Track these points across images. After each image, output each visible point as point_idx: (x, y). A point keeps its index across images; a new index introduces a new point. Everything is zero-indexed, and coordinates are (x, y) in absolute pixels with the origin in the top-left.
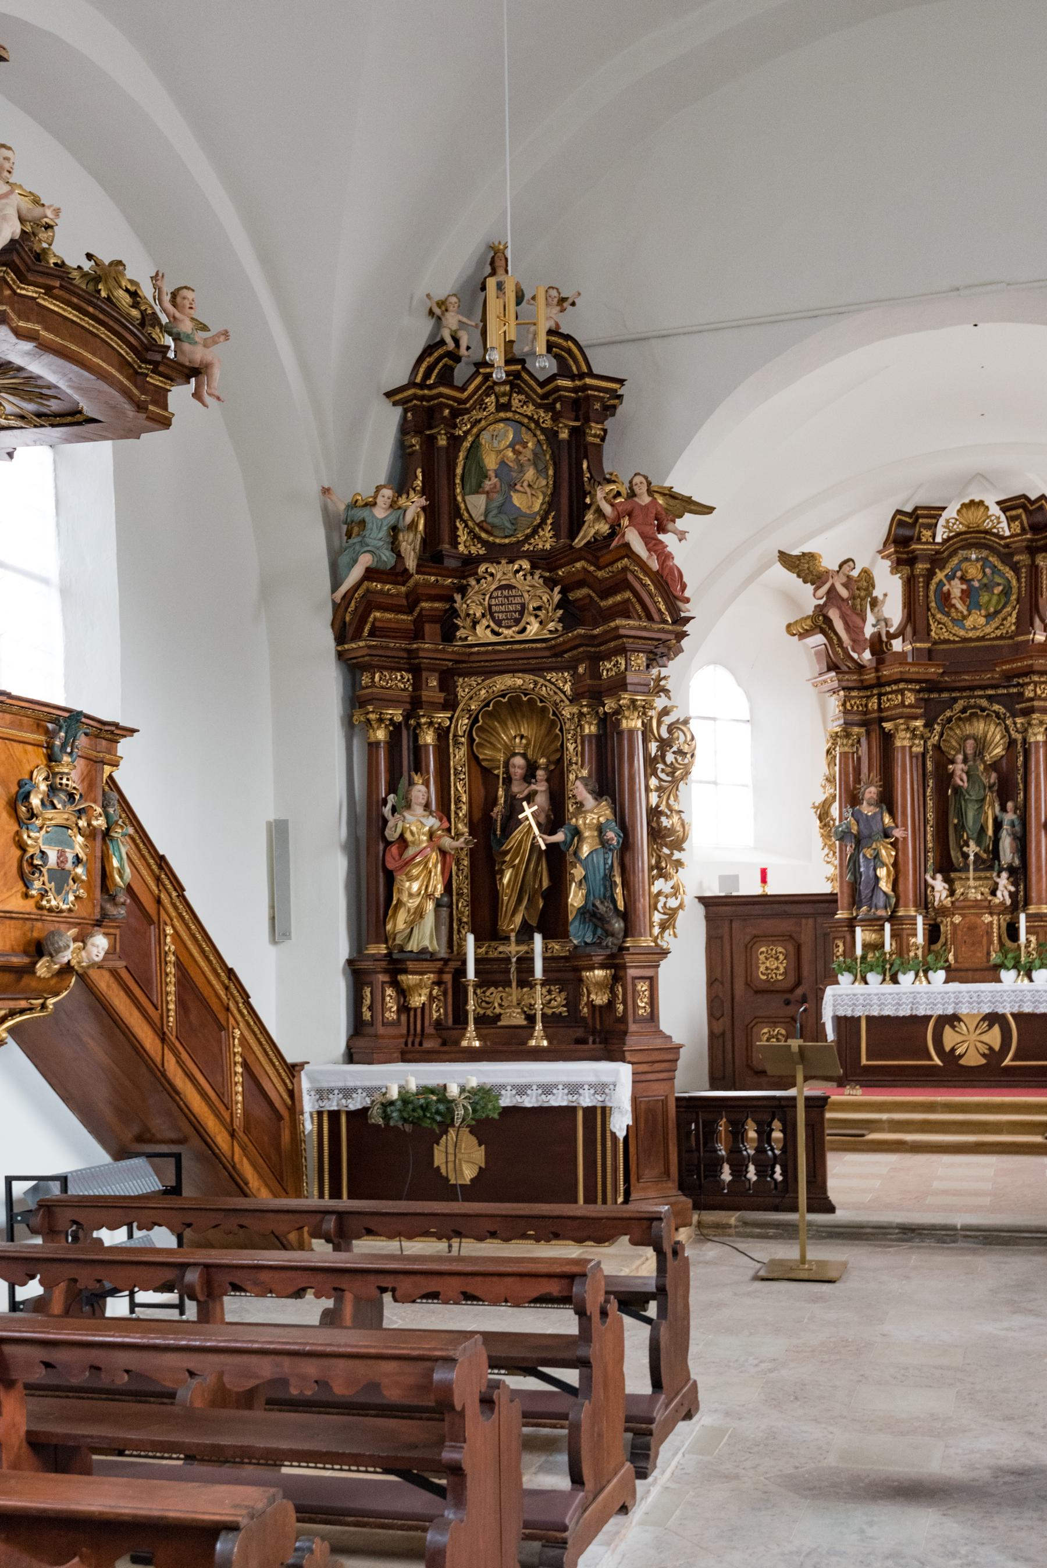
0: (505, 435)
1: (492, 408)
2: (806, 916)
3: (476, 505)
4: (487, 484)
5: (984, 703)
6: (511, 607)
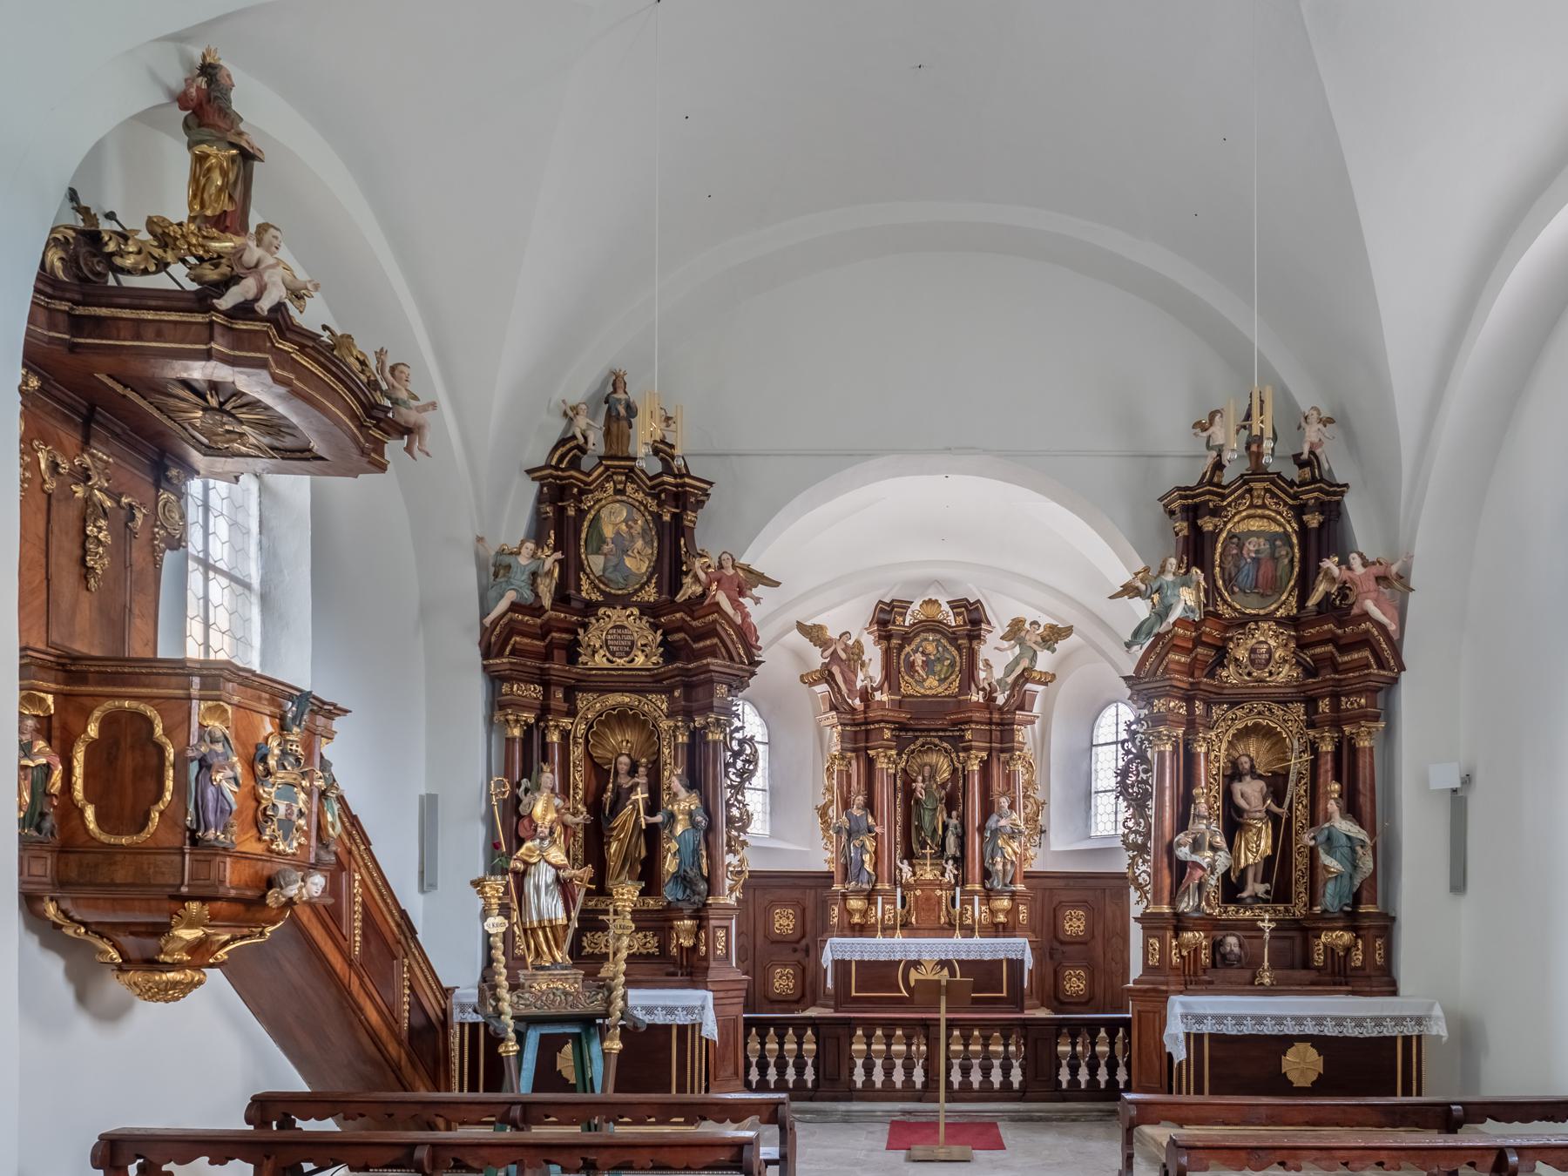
0: (621, 512)
1: (611, 491)
2: (810, 888)
3: (596, 563)
4: (606, 548)
5: (937, 741)
6: (621, 641)
